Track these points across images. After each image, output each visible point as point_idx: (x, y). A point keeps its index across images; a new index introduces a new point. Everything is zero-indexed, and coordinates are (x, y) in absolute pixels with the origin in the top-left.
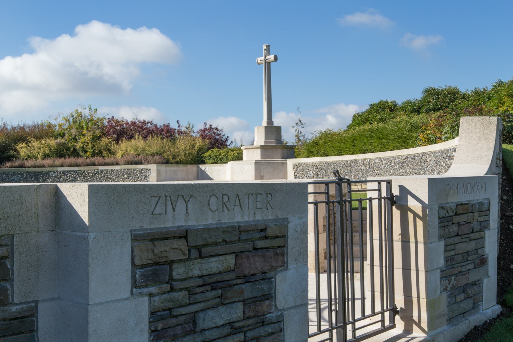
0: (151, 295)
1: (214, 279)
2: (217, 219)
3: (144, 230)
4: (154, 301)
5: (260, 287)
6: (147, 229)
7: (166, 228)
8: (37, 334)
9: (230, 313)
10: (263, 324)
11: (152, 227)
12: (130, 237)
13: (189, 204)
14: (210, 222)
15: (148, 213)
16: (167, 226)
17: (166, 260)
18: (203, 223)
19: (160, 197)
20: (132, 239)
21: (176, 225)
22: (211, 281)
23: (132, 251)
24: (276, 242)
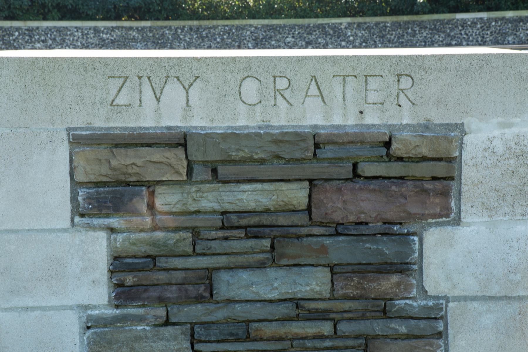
0: (112, 230)
1: (254, 220)
2: (259, 119)
3: (95, 129)
4: (115, 240)
5: (374, 247)
6: (101, 129)
7: (140, 128)
8: (421, 280)
9: (295, 282)
10: (385, 314)
11: (112, 125)
12: (65, 137)
13: (191, 91)
14: (242, 122)
15: (101, 104)
16: (143, 125)
17: (139, 179)
18: (227, 125)
19: (127, 77)
20: (70, 142)
21: (164, 125)
22: (244, 222)
23: (71, 160)
24: (440, 169)
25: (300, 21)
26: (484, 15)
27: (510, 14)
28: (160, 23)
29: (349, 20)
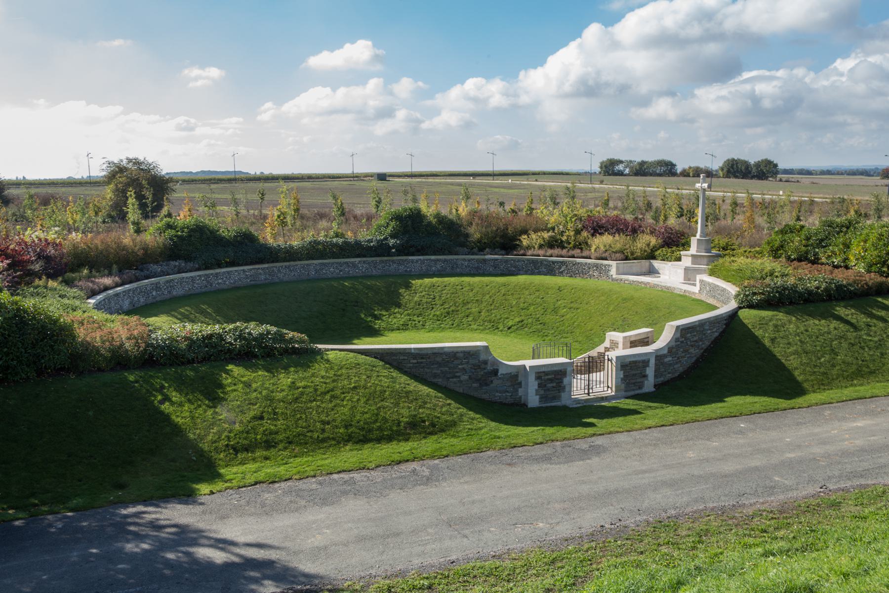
25: (336, 260)
26: (421, 257)
27: (433, 257)
28: (272, 265)
29: (359, 259)
